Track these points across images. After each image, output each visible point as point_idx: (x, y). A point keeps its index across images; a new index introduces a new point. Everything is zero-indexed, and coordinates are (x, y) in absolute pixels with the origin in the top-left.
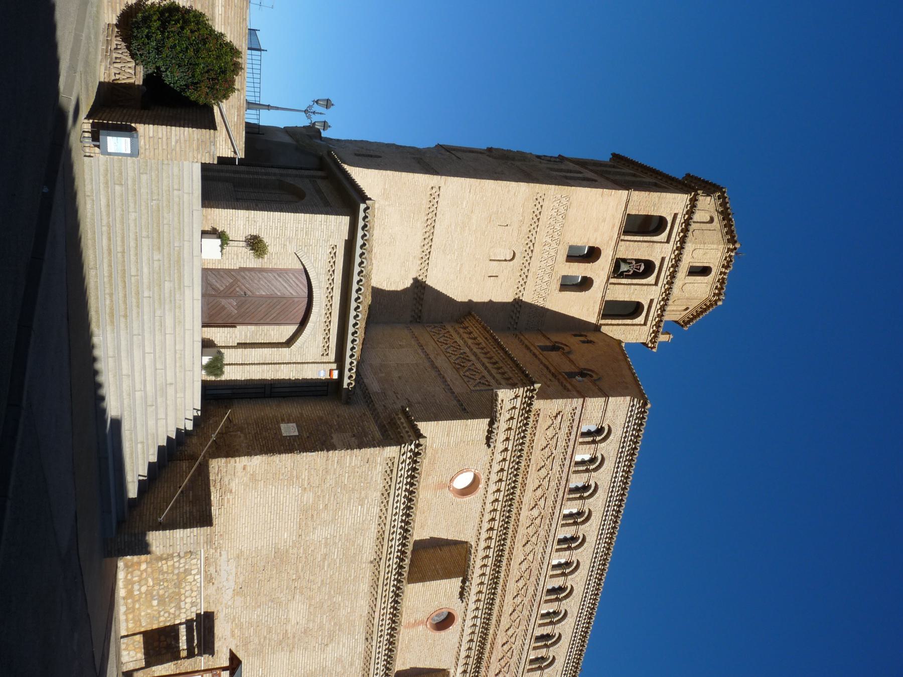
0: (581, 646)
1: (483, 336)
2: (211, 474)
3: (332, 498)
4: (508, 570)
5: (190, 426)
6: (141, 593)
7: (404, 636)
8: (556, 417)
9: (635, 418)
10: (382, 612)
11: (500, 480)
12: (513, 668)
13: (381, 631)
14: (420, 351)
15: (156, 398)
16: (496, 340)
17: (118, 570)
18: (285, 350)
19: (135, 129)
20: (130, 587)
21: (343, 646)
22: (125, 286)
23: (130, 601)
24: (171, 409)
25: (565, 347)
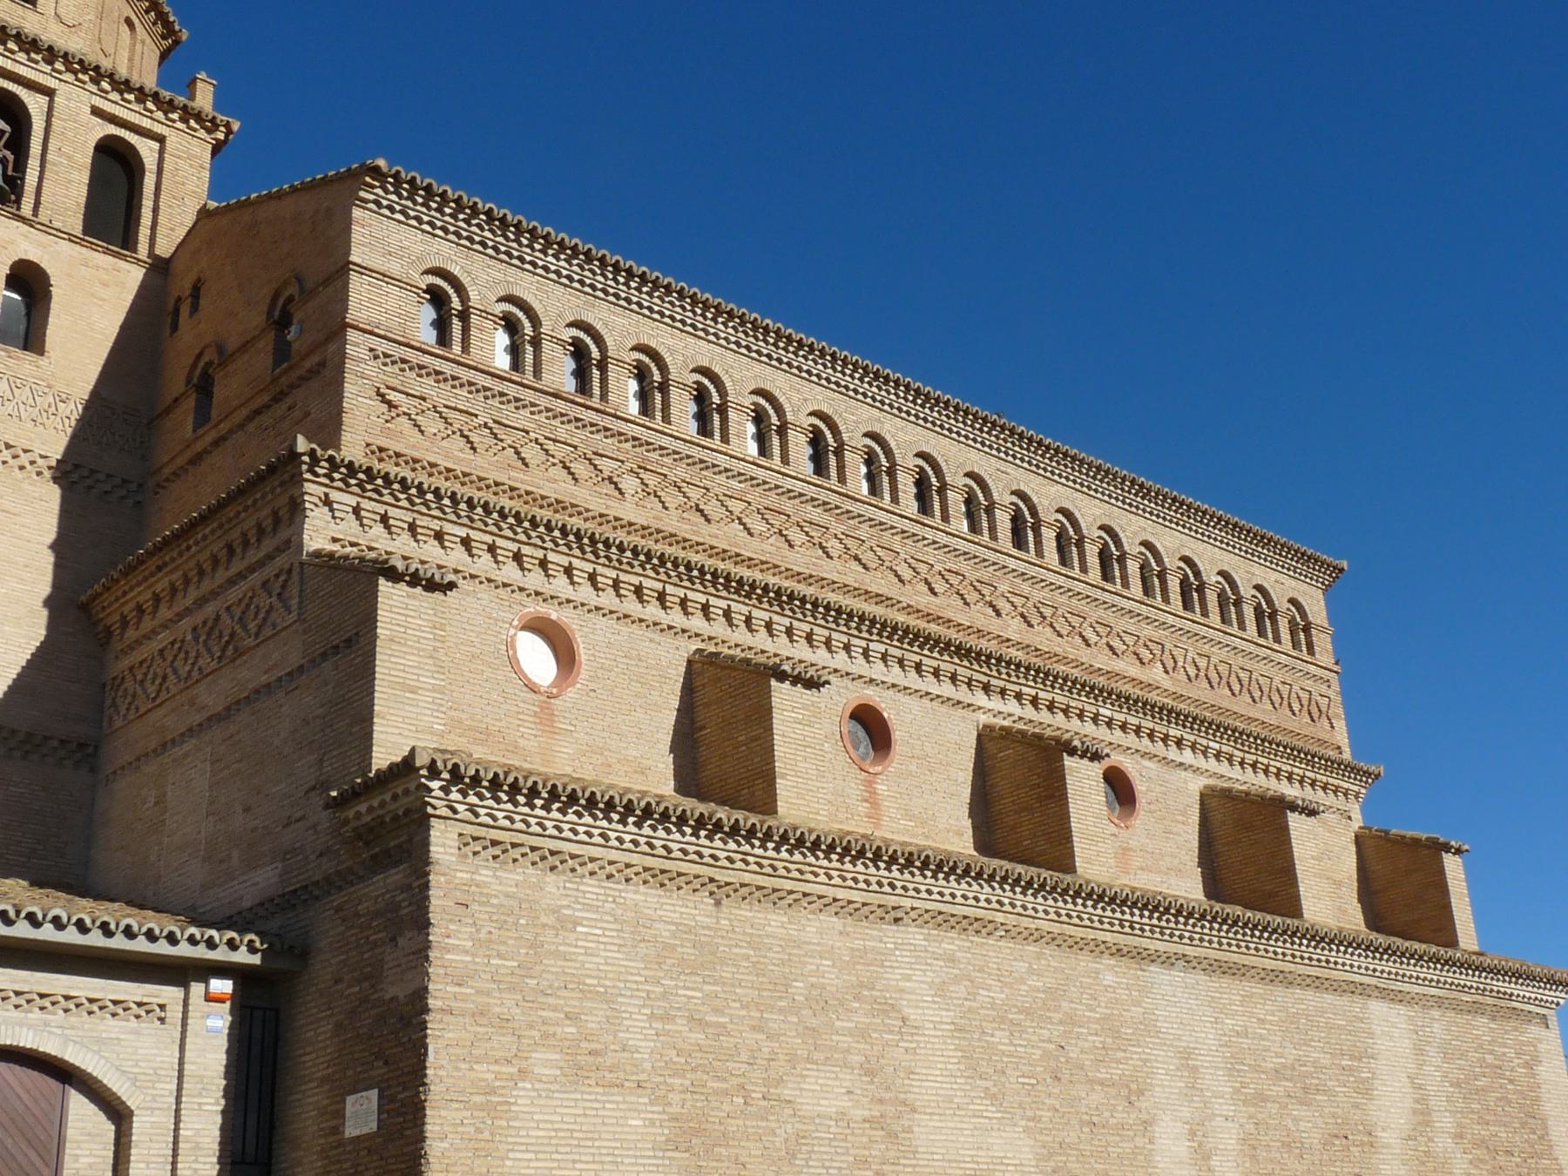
0: (946, 408)
1: (152, 575)
3: (551, 1000)
7: (896, 831)
8: (391, 405)
9: (409, 203)
10: (837, 881)
11: (543, 564)
12: (986, 574)
13: (880, 884)
14: (178, 751)
16: (166, 542)
18: (140, 1126)
21: (908, 978)
25: (206, 358)
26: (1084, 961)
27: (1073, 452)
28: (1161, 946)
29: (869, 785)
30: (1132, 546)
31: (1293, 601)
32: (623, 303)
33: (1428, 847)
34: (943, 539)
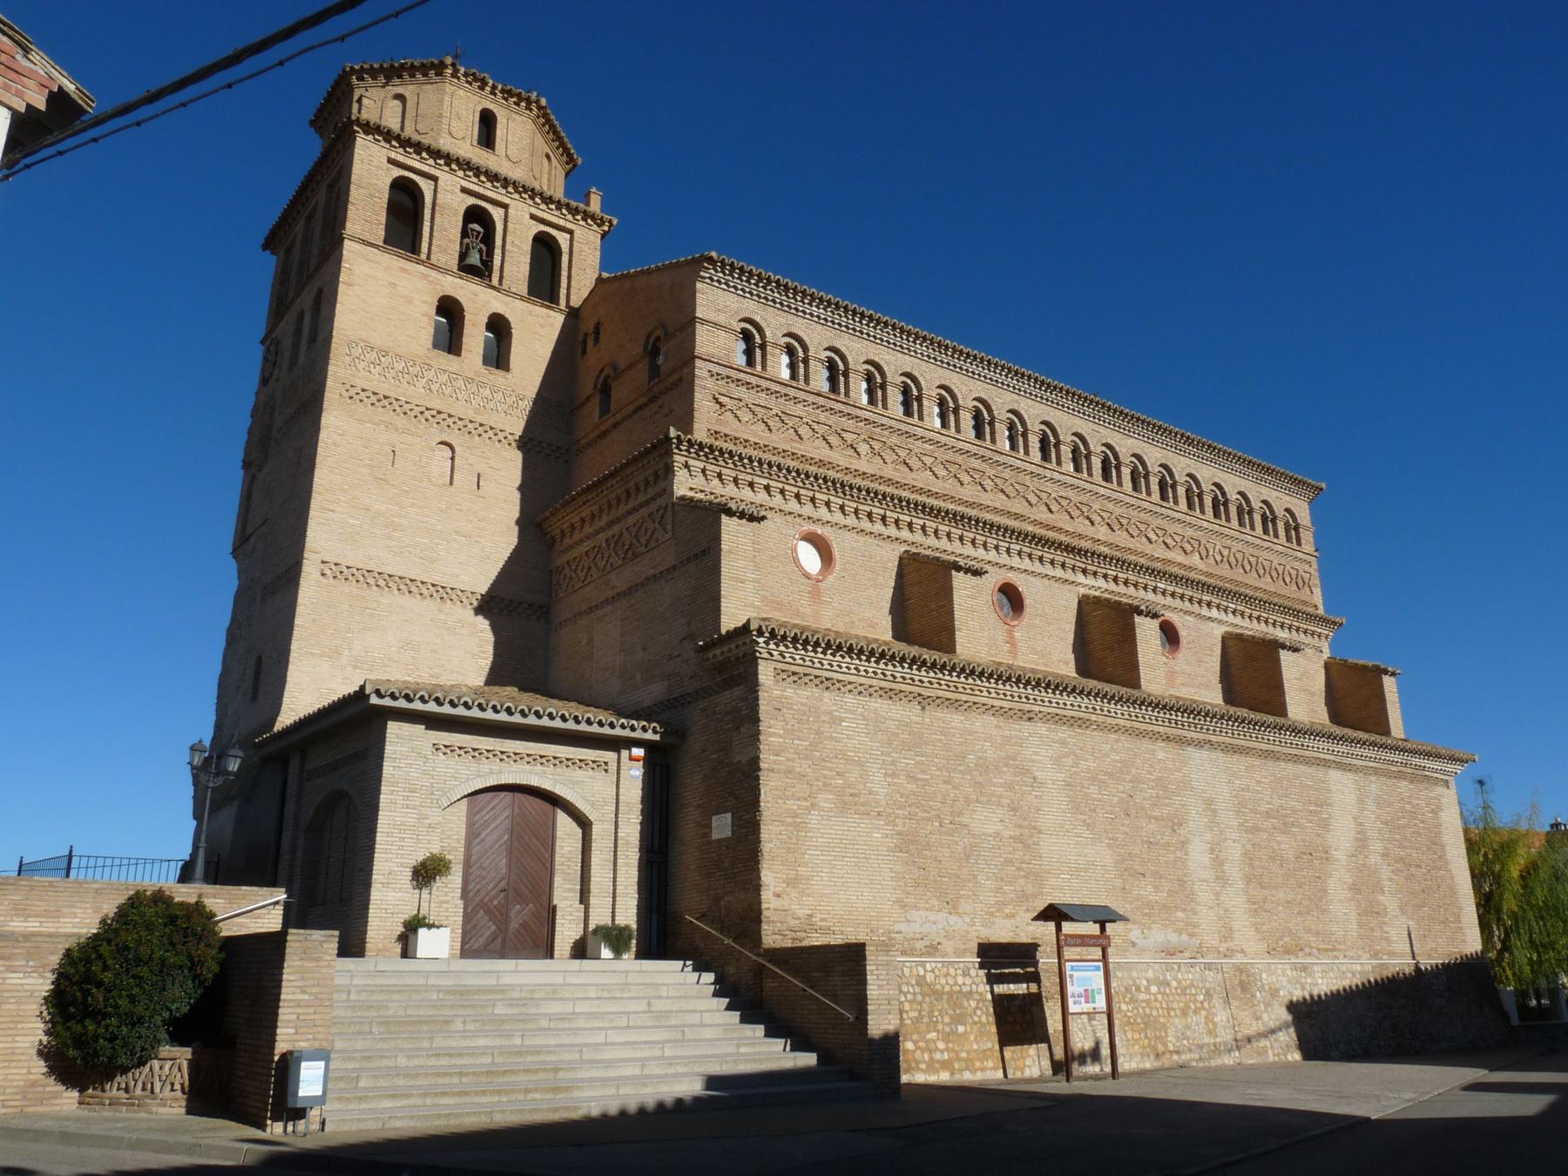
0: (1061, 392)
1: (580, 507)
2: (784, 945)
3: (829, 765)
4: (945, 497)
5: (709, 977)
6: (947, 1049)
7: (1026, 661)
8: (721, 405)
9: (730, 278)
10: (994, 695)
11: (813, 500)
12: (1084, 498)
13: (1020, 697)
14: (600, 613)
15: (672, 1026)
16: (589, 488)
17: (913, 1082)
18: (596, 830)
19: (284, 1056)
20: (937, 1065)
21: (1037, 754)
22: (511, 1071)
23: (957, 1066)
24: (685, 1005)
25: (605, 373)
26: (1146, 745)
27: (1143, 417)
28: (1195, 735)
29: (1010, 632)
30: (1180, 477)
31: (1287, 510)
32: (858, 334)
33: (1374, 671)
34: (1056, 476)
